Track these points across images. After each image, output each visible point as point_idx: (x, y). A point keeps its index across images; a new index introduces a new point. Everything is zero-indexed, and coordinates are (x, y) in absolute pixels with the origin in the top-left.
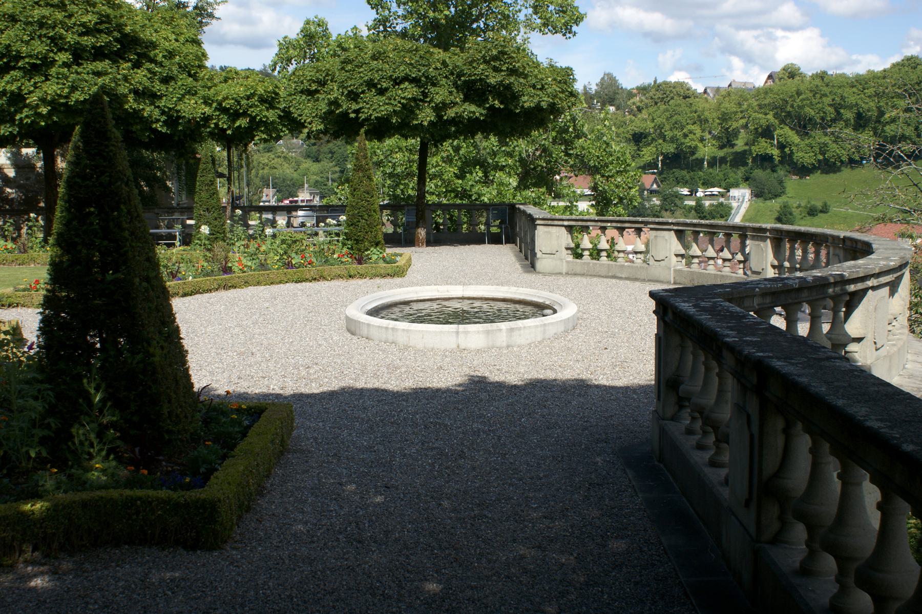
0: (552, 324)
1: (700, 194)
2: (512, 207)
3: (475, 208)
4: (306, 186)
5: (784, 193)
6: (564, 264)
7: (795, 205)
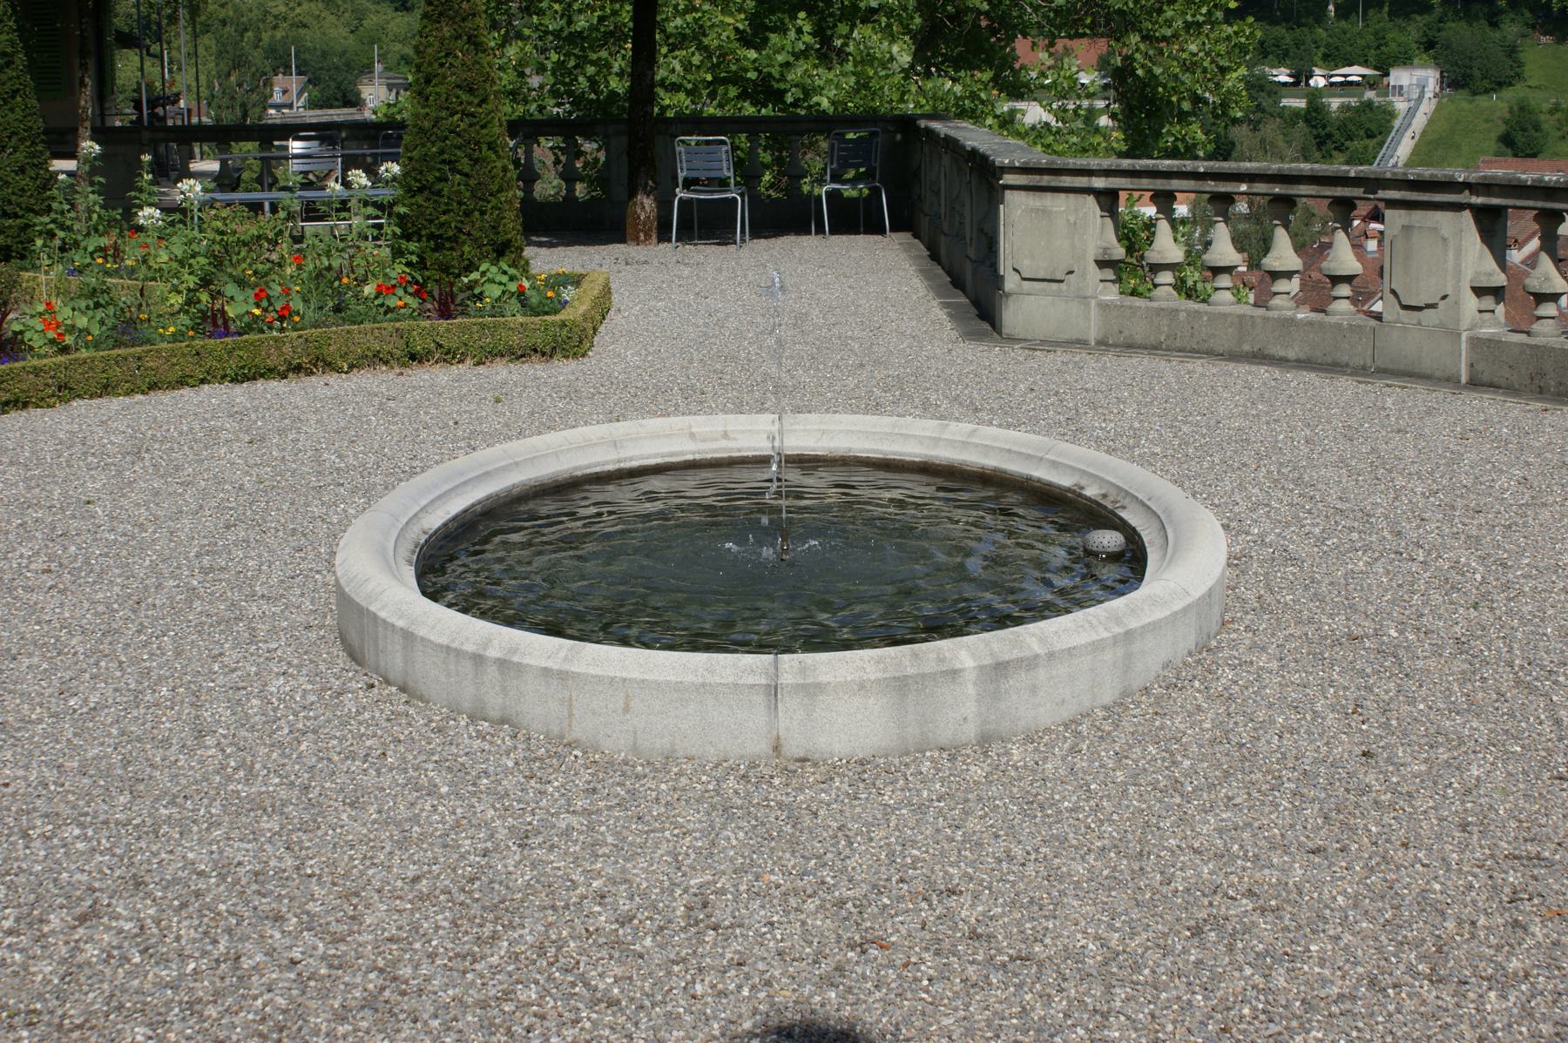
0: (1154, 626)
1: (1318, 81)
2: (906, 123)
3: (792, 127)
4: (378, 67)
5: (1519, 76)
6: (1094, 312)
7: (1546, 106)
